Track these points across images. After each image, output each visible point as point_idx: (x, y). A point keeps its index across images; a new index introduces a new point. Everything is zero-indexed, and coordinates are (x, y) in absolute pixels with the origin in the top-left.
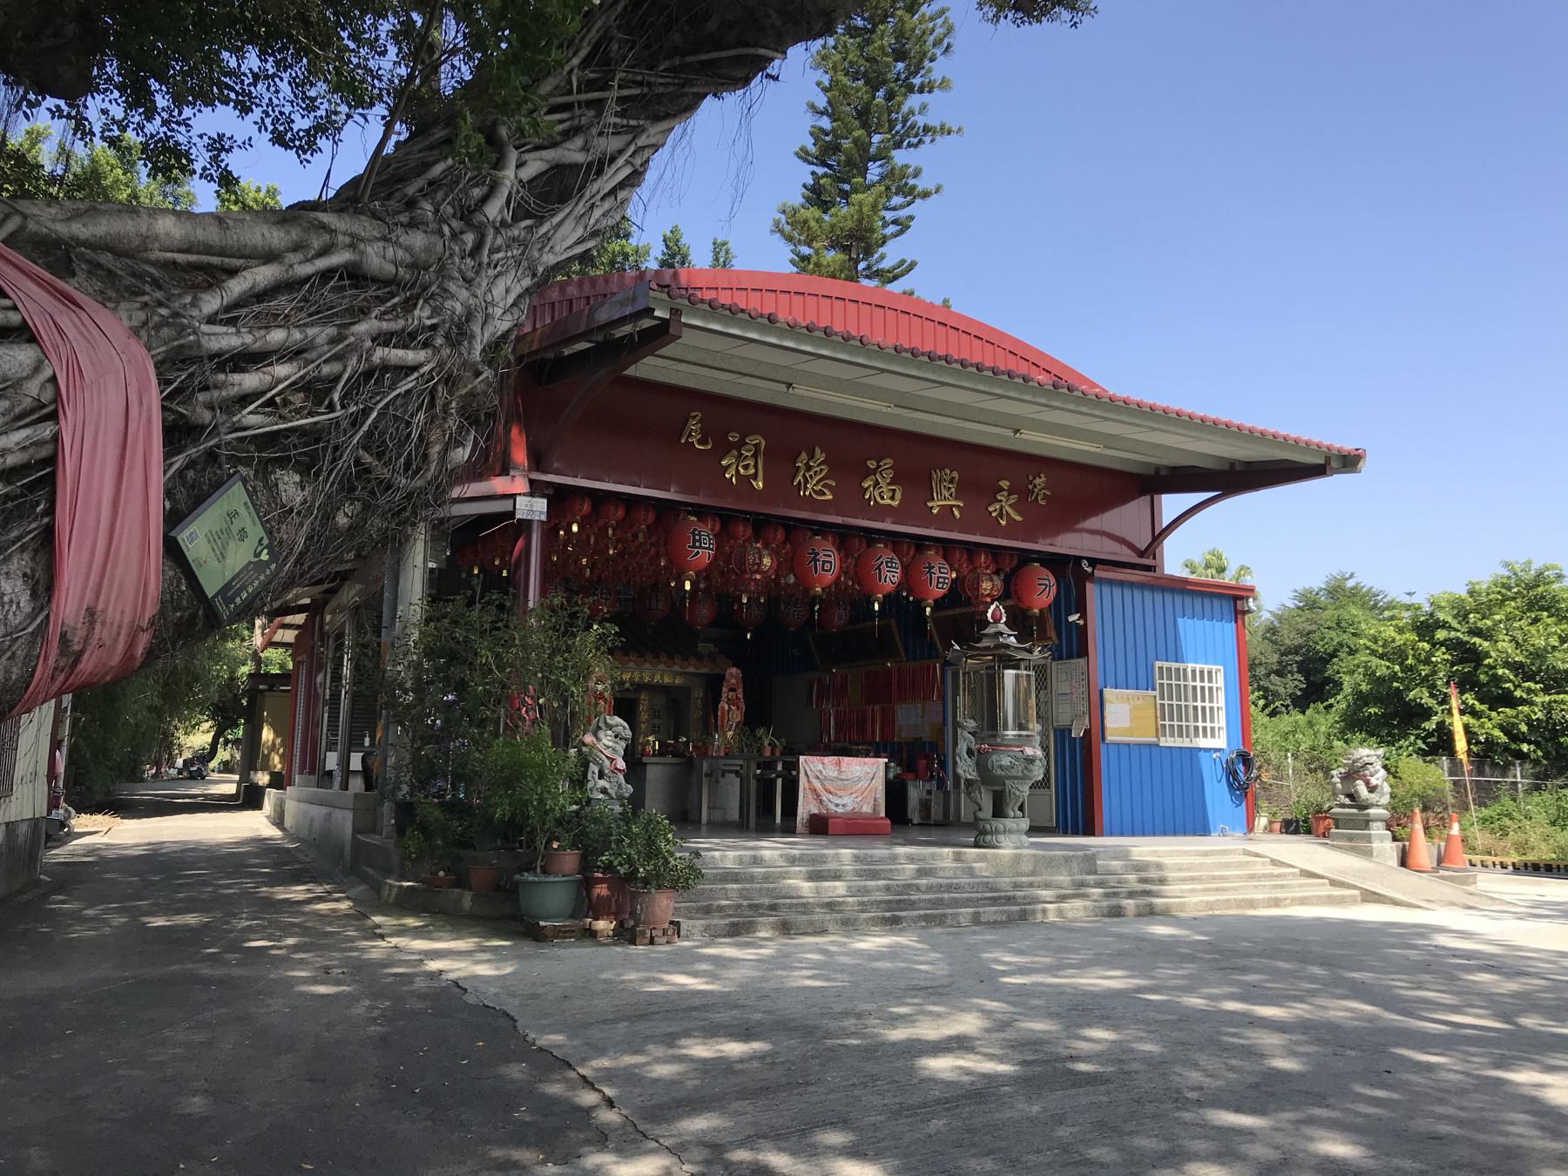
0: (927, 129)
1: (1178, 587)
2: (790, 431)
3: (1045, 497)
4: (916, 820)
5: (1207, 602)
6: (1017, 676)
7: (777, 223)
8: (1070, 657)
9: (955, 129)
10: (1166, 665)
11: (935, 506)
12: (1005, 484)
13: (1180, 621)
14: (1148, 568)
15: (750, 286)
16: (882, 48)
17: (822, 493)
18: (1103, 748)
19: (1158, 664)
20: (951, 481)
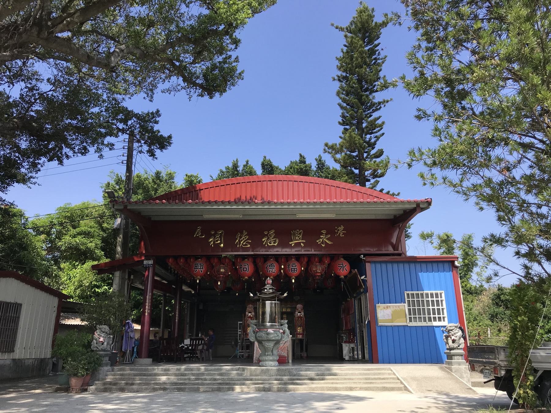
0: (380, 103)
1: (414, 260)
2: (231, 228)
3: (343, 234)
4: (347, 358)
5: (407, 266)
6: (271, 304)
7: (325, 150)
8: (13, 304)
9: (389, 100)
10: (410, 292)
11: (319, 241)
12: (324, 232)
13: (420, 274)
14: (400, 255)
15: (257, 180)
16: (354, 83)
17: (246, 245)
18: (378, 330)
19: (406, 293)
20: (300, 234)
